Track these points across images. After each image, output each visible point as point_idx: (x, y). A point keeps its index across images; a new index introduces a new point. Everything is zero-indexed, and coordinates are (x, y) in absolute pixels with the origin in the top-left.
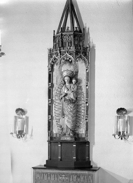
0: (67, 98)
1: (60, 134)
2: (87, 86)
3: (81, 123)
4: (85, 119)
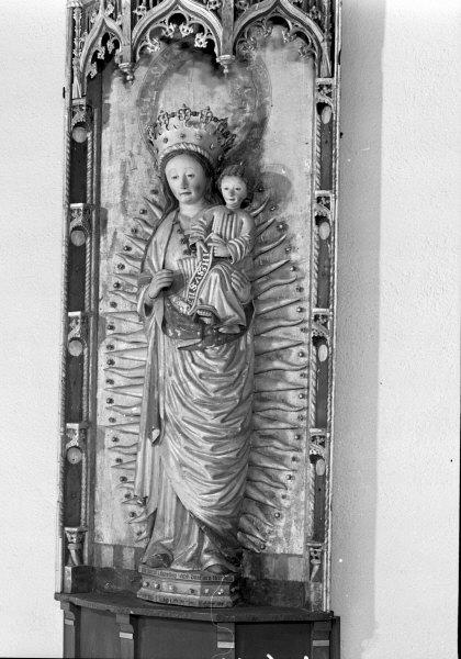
0: (183, 308)
1: (139, 553)
2: (320, 220)
3: (283, 477)
4: (303, 455)
